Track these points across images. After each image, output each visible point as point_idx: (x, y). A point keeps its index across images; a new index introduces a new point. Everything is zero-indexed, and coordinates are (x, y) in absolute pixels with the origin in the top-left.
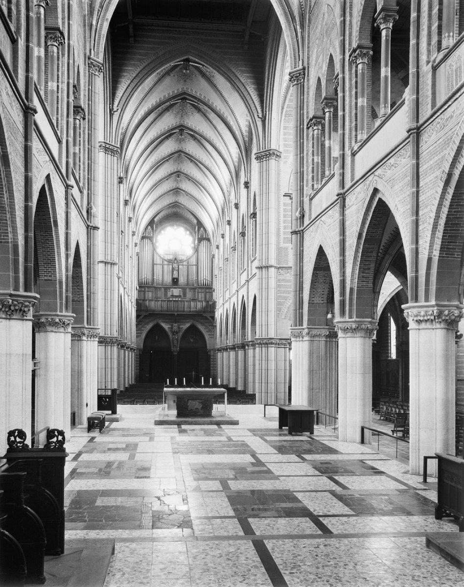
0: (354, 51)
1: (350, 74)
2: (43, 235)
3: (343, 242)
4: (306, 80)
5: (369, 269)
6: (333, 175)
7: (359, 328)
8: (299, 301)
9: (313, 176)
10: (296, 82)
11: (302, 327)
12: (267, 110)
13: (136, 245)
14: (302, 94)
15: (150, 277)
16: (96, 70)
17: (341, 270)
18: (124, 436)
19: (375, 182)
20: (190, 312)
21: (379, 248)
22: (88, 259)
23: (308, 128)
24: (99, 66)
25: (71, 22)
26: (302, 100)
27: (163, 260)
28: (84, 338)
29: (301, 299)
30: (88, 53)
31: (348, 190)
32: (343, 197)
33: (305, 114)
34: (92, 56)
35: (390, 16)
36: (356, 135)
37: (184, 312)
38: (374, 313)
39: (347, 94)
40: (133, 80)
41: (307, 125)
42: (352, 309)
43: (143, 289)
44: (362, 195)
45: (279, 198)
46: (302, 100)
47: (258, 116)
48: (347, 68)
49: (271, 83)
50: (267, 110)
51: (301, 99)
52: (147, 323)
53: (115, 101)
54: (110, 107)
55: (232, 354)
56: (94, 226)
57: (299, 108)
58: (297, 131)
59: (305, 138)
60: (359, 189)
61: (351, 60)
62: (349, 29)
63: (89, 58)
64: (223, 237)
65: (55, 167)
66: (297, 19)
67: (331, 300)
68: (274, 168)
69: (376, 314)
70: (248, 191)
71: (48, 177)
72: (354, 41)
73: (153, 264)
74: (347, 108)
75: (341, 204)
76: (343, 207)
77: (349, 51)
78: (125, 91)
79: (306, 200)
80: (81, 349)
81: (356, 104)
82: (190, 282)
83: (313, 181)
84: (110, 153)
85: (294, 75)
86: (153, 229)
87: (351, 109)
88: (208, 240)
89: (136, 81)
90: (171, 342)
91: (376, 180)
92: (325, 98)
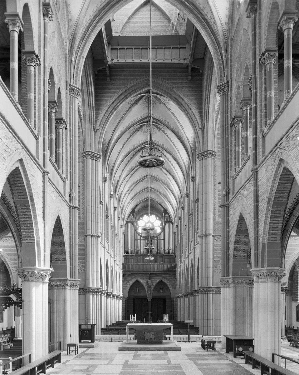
0: (263, 54)
1: (261, 74)
2: (23, 208)
3: (256, 208)
4: (229, 91)
5: (278, 227)
6: (249, 158)
7: (270, 275)
8: (227, 258)
9: (235, 162)
10: (222, 93)
11: (228, 277)
12: (205, 122)
13: (121, 227)
14: (227, 102)
15: (132, 248)
16: (75, 93)
17: (255, 229)
18: (91, 359)
19: (280, 154)
20: (159, 271)
21: (285, 210)
22: (70, 230)
23: (231, 126)
24: (77, 90)
25: (46, 50)
26: (227, 106)
27: (141, 236)
28: (67, 287)
29: (228, 255)
30: (69, 81)
31: (260, 165)
32: (256, 172)
33: (229, 115)
34: (72, 83)
35: (290, 19)
36: (266, 121)
37: (155, 271)
38: (282, 263)
39: (258, 90)
40: (110, 107)
41: (231, 124)
42: (264, 260)
43: (128, 257)
44: (270, 167)
45: (215, 185)
46: (227, 106)
47: (199, 127)
48: (258, 70)
49: (207, 102)
50: (205, 122)
51: (226, 105)
52: (131, 280)
53: (98, 122)
54: (94, 127)
55: (186, 299)
56: (75, 206)
57: (225, 112)
58: (223, 130)
59: (229, 134)
60: (270, 160)
61: (261, 62)
62: (259, 39)
63: (70, 85)
64: (180, 219)
65: (28, 154)
66: (222, 45)
67: (249, 256)
68: (211, 164)
69: (283, 264)
70: (194, 183)
71: (21, 161)
72: (263, 47)
73: (134, 240)
74: (258, 100)
75: (254, 178)
76: (256, 180)
77: (259, 56)
78: (104, 115)
79: (231, 180)
80: (65, 295)
81: (266, 96)
82: (160, 252)
83: (236, 166)
84: (94, 159)
85: (220, 88)
86: (134, 216)
87: (262, 101)
88: (171, 222)
89: (112, 108)
90: (147, 292)
91: (281, 152)
92: (243, 100)
